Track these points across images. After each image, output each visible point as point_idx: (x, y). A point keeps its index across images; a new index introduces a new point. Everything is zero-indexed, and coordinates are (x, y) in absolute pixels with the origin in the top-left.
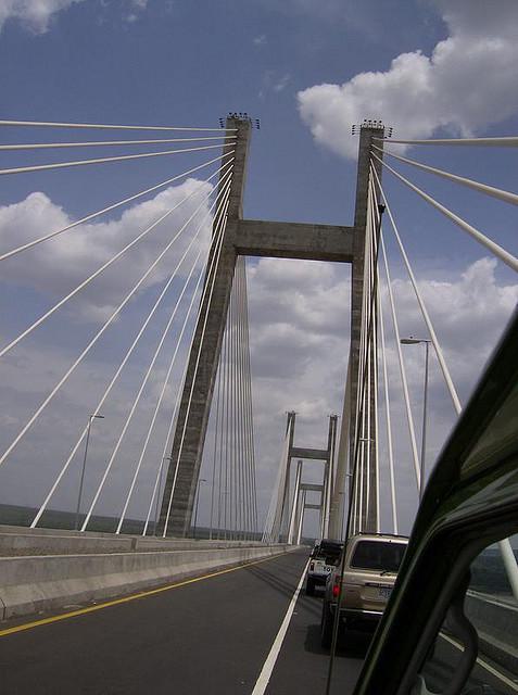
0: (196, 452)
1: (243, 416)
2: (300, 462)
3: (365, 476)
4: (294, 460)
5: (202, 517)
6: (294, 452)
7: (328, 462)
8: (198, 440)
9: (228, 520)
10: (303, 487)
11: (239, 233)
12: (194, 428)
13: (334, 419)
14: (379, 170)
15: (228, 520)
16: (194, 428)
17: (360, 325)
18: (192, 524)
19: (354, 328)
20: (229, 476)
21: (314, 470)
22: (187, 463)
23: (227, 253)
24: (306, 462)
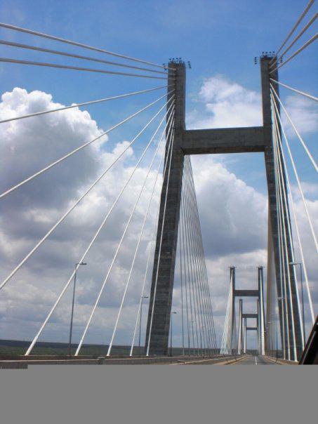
0: (168, 293)
1: (199, 280)
2: (241, 300)
3: (287, 279)
4: (237, 298)
5: (176, 340)
6: (236, 293)
7: (260, 298)
8: (168, 284)
9: (196, 342)
10: (245, 316)
11: (183, 140)
12: (165, 276)
13: (260, 269)
14: (276, 86)
15: (196, 342)
16: (165, 276)
17: (275, 194)
18: (169, 346)
19: (271, 196)
20: (192, 299)
21: (250, 305)
22: (159, 333)
23: (177, 153)
24: (244, 298)
